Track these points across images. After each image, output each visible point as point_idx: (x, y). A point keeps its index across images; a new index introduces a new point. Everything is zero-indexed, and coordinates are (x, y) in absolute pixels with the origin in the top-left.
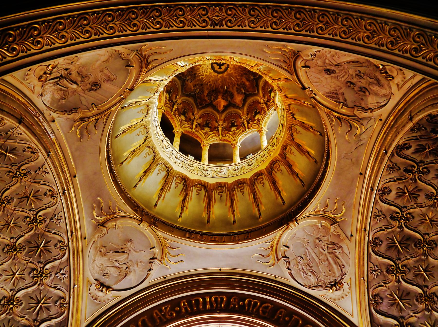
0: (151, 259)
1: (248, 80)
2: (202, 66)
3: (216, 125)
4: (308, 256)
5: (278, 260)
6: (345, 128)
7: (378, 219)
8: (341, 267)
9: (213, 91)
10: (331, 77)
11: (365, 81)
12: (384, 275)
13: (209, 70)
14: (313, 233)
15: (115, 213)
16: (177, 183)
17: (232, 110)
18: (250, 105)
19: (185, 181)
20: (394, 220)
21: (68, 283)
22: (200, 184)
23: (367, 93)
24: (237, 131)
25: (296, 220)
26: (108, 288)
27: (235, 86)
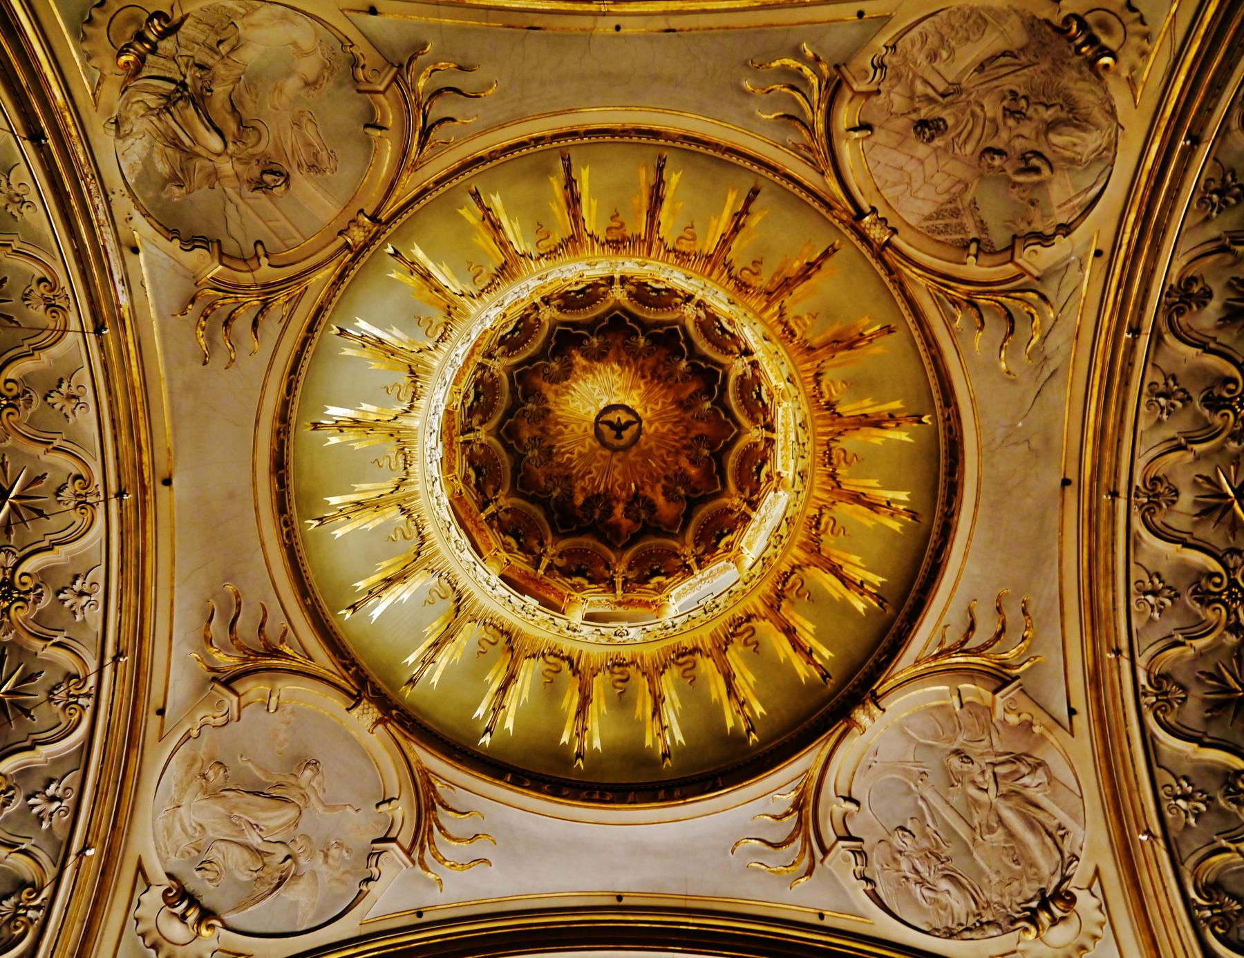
0: (374, 841)
1: (693, 462)
4: (929, 821)
5: (825, 852)
6: (995, 328)
7: (1152, 606)
8: (1056, 836)
9: (599, 495)
10: (935, 149)
11: (1033, 125)
12: (1221, 811)
14: (936, 737)
15: (276, 653)
17: (652, 542)
19: (510, 640)
20: (1208, 605)
21: (61, 835)
23: (1046, 172)
25: (876, 699)
26: (207, 915)
27: (658, 481)
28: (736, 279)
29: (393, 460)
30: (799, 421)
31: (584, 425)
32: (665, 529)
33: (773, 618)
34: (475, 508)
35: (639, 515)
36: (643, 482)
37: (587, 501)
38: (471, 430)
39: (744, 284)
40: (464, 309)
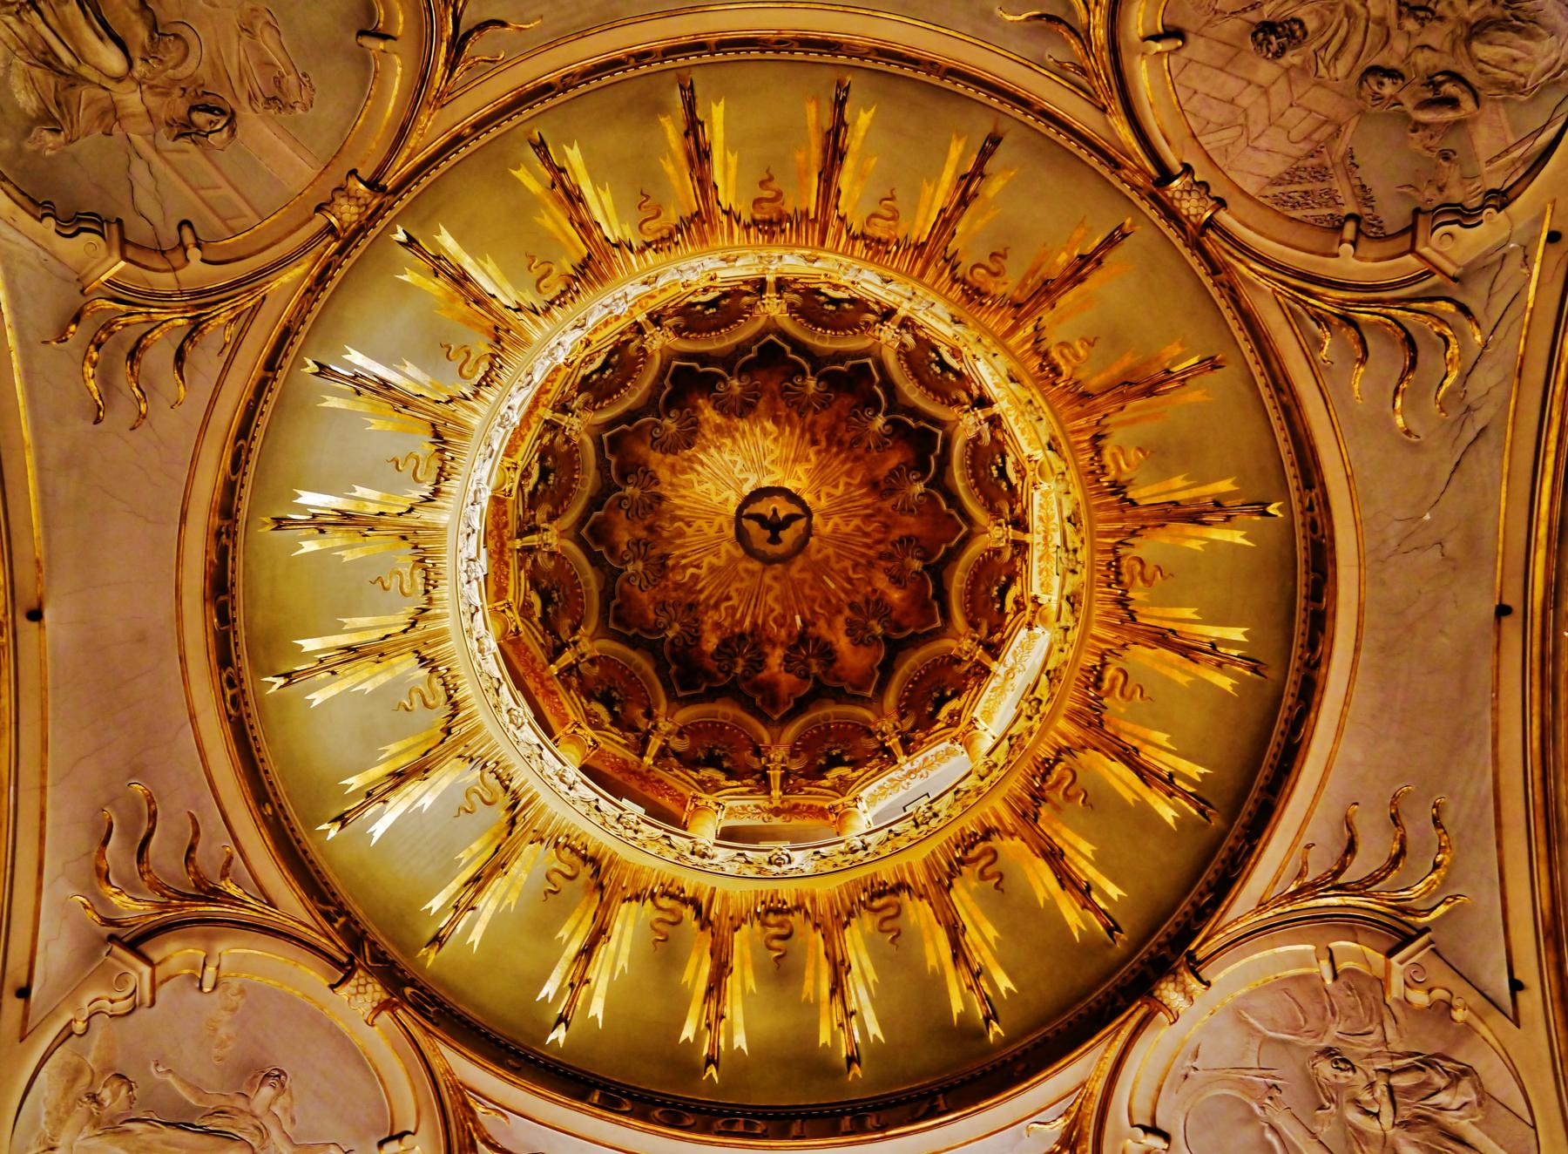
1: (897, 581)
2: (695, 526)
6: (1386, 359)
9: (742, 636)
14: (1296, 1030)
15: (216, 896)
17: (829, 711)
22: (672, 897)
23: (1468, 104)
27: (839, 612)
28: (964, 282)
29: (407, 578)
30: (1067, 513)
33: (1026, 834)
34: (541, 656)
35: (809, 666)
36: (813, 612)
37: (724, 643)
38: (534, 530)
39: (977, 291)
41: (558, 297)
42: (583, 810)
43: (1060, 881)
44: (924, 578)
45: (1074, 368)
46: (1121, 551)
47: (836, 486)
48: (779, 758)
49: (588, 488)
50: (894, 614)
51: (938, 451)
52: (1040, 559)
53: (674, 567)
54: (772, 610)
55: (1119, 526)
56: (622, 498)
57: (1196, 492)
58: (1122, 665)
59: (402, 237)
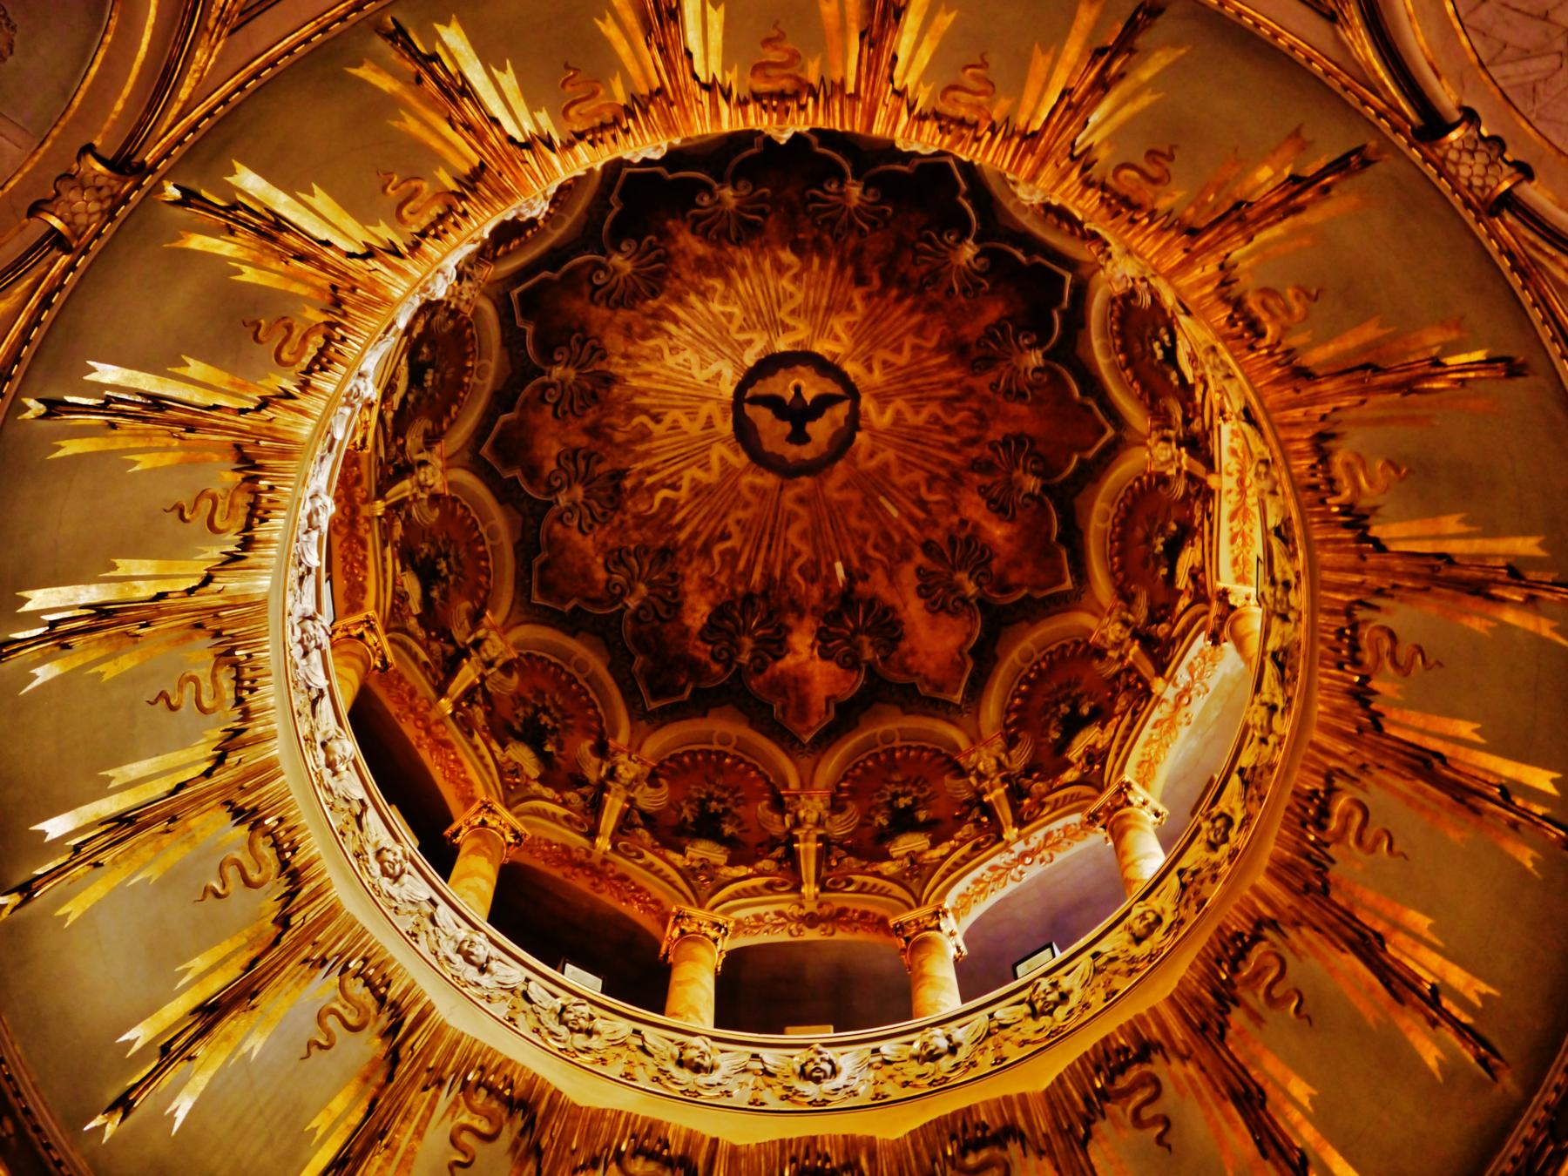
1: (1000, 509)
2: (668, 420)
3: (778, 826)
9: (749, 598)
13: (719, 451)
16: (466, 1138)
17: (893, 725)
18: (1026, 680)
19: (530, 1124)
22: (650, 1156)
24: (937, 853)
27: (907, 556)
28: (1104, 187)
29: (206, 685)
30: (1272, 522)
31: (705, 409)
32: (925, 690)
33: (1206, 1059)
34: (419, 681)
35: (858, 648)
36: (864, 558)
37: (719, 613)
38: (405, 470)
39: (1125, 201)
40: (373, 286)
41: (433, 225)
42: (501, 1010)
43: (1259, 1144)
44: (1043, 505)
45: (1285, 330)
46: (1361, 614)
47: (898, 350)
48: (814, 817)
49: (489, 380)
50: (995, 563)
51: (1065, 304)
52: (1233, 517)
53: (635, 489)
54: (797, 554)
55: (1357, 579)
56: (545, 387)
57: (1478, 546)
58: (1361, 796)
59: (172, 192)
